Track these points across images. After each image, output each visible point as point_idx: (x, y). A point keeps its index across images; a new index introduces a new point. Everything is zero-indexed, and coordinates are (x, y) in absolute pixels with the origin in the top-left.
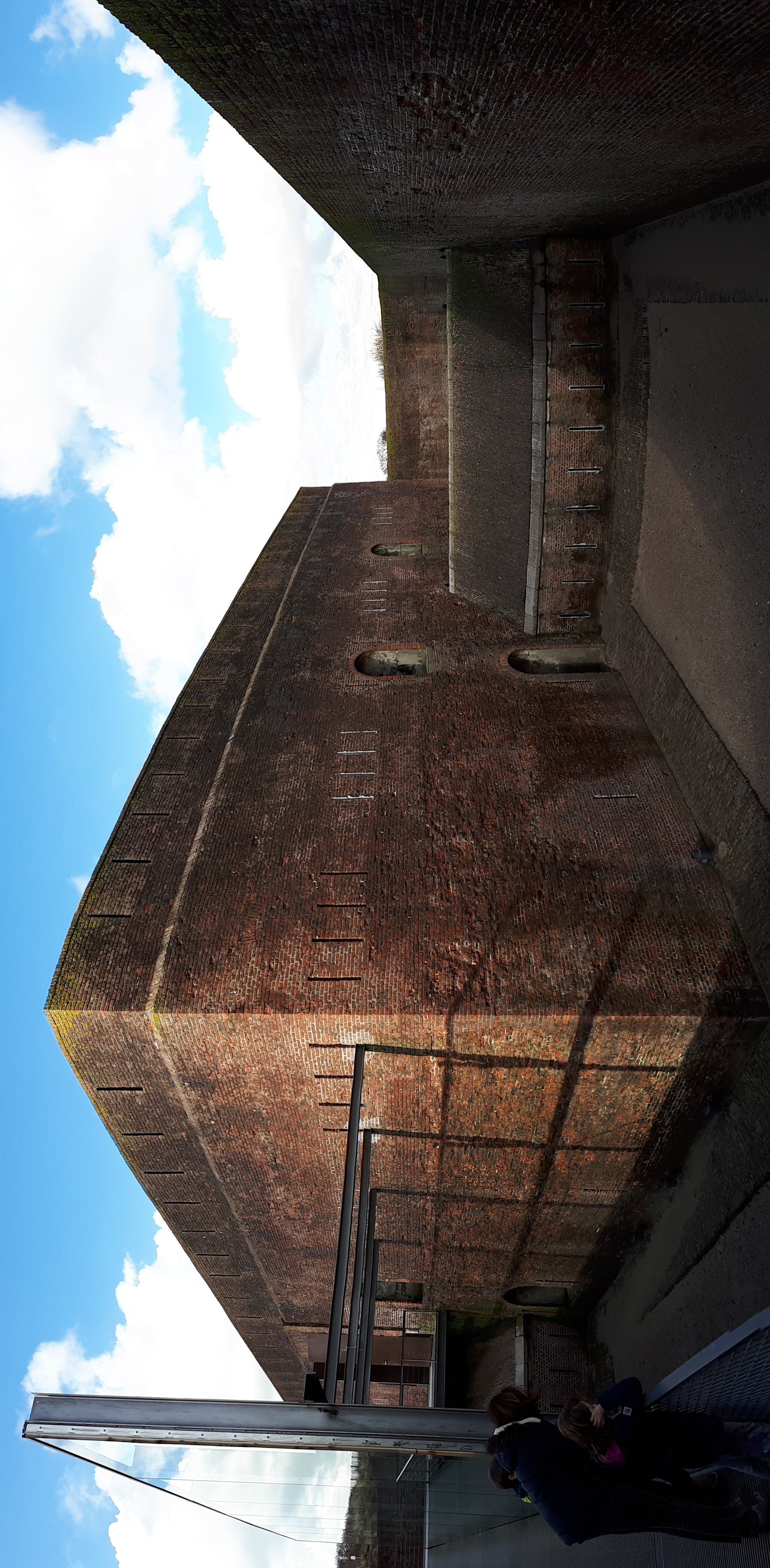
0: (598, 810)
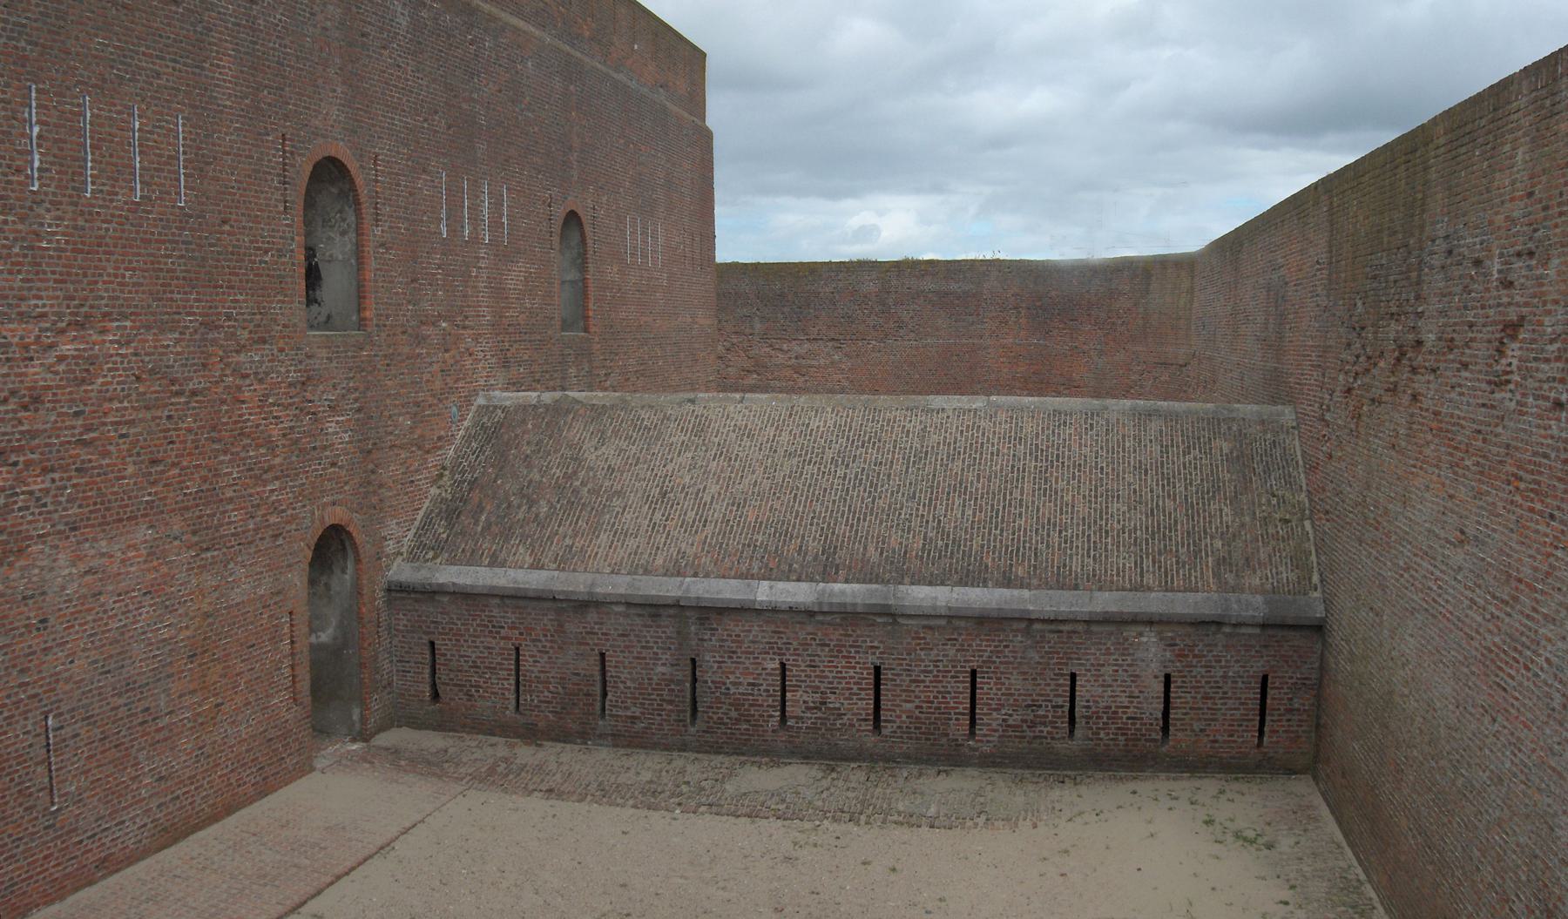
0: (22, 722)
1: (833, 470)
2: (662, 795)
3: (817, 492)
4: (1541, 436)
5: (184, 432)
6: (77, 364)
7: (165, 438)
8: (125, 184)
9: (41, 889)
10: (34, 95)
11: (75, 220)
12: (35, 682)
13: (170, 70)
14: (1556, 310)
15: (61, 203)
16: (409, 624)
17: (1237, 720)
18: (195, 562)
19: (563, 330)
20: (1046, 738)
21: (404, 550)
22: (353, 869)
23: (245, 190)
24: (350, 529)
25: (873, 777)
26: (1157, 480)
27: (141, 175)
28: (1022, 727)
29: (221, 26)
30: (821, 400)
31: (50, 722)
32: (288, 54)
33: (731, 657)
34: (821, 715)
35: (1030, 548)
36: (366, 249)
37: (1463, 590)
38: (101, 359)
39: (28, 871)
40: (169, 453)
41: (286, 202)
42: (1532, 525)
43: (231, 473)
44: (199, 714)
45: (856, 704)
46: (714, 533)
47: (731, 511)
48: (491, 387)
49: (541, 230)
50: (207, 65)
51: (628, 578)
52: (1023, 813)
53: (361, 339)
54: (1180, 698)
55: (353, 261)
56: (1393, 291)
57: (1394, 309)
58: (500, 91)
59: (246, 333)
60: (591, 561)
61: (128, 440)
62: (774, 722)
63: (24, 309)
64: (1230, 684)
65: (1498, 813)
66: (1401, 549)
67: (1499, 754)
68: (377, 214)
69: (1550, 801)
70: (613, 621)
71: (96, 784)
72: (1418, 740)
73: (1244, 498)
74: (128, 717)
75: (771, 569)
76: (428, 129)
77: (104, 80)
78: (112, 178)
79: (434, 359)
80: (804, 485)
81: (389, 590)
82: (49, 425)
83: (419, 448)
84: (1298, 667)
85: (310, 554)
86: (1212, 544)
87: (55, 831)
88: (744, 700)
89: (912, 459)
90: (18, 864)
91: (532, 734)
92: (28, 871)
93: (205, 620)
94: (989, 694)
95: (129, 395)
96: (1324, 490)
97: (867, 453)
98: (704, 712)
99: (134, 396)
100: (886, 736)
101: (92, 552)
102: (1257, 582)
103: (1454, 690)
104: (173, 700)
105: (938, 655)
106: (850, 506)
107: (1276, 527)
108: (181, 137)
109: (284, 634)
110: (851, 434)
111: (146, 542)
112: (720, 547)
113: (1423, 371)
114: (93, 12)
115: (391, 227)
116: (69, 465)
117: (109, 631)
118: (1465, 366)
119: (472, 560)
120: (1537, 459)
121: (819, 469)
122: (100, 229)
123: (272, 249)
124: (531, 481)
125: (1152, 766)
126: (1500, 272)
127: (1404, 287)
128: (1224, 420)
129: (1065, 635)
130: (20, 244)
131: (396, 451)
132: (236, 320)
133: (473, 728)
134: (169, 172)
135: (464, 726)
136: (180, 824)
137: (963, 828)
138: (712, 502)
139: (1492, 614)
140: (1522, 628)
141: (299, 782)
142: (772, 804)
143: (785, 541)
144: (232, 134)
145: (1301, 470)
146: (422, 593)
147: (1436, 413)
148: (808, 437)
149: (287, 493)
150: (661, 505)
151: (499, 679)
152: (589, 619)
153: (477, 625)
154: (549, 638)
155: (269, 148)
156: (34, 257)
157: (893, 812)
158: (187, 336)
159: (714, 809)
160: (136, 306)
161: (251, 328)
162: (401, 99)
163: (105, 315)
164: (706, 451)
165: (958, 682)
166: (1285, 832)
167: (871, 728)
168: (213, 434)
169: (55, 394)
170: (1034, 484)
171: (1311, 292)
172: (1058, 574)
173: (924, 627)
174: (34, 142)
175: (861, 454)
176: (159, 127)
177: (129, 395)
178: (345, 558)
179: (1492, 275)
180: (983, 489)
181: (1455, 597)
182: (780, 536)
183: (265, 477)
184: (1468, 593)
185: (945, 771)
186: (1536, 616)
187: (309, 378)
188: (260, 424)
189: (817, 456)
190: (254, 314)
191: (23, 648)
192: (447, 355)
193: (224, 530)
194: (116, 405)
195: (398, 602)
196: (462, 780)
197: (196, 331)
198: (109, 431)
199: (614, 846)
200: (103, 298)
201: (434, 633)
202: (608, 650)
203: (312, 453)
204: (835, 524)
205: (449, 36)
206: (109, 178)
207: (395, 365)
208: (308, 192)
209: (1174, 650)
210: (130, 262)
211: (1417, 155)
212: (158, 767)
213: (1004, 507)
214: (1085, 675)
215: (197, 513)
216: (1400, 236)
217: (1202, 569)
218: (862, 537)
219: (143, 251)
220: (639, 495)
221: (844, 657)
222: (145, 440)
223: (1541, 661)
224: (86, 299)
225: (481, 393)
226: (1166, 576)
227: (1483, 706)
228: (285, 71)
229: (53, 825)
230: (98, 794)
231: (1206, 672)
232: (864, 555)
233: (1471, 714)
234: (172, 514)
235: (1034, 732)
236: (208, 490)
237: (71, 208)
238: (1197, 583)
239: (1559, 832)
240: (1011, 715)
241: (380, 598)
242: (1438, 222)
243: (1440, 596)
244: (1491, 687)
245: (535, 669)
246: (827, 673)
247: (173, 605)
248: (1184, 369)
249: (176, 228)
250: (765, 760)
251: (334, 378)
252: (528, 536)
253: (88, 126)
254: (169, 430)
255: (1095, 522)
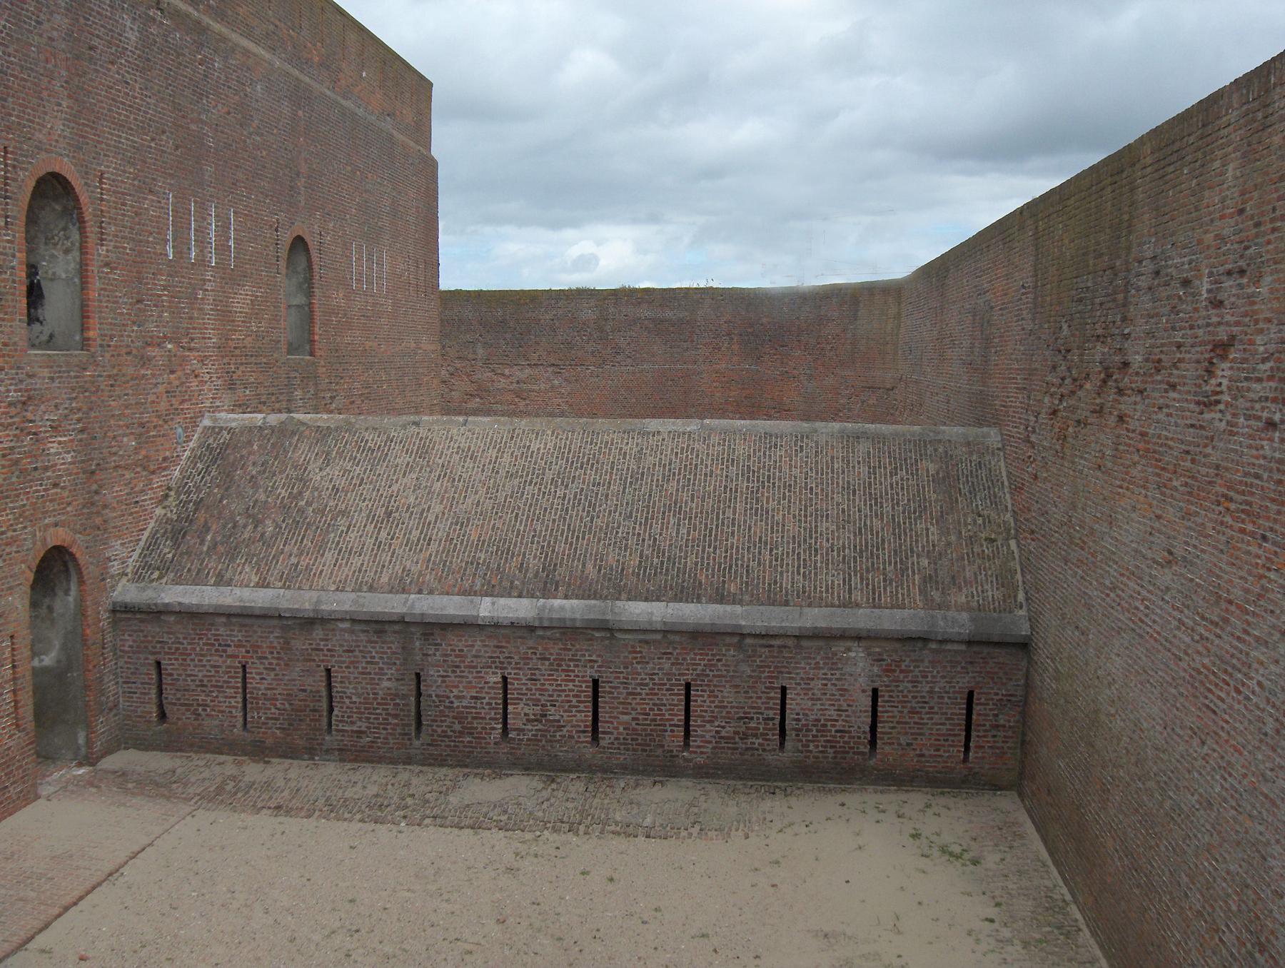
2: (389, 809)
3: (537, 512)
4: (1252, 456)
14: (1268, 329)
16: (135, 645)
17: (943, 735)
20: (757, 750)
22: (81, 898)
24: (74, 550)
25: (591, 787)
26: (865, 501)
28: (734, 738)
30: (541, 423)
33: (454, 672)
35: (742, 565)
37: (1170, 610)
41: (7, 217)
42: (1244, 546)
45: (575, 716)
46: (438, 551)
47: (455, 530)
48: (218, 409)
49: (267, 255)
51: (353, 595)
52: (735, 823)
53: (85, 360)
54: (887, 712)
55: (76, 280)
56: (1098, 313)
57: (1100, 332)
64: (936, 699)
65: (1207, 838)
66: (1108, 569)
67: (1209, 778)
68: (102, 233)
69: (1262, 828)
72: (1124, 760)
73: (950, 518)
75: (494, 586)
76: (155, 149)
79: (159, 380)
80: (525, 505)
81: (114, 611)
83: (145, 469)
84: (1003, 684)
85: (31, 576)
86: (918, 563)
89: (629, 480)
91: (260, 751)
94: (703, 706)
96: (1029, 510)
97: (585, 474)
98: (428, 725)
100: (604, 748)
102: (963, 599)
103: (1162, 711)
105: (654, 669)
106: (569, 525)
107: (982, 546)
109: (6, 659)
113: (1129, 392)
115: (115, 247)
118: (1173, 387)
120: (1249, 480)
121: (540, 489)
125: (860, 779)
126: (1209, 291)
127: (1110, 309)
128: (930, 442)
129: (776, 649)
131: (120, 472)
133: (201, 747)
135: (192, 746)
137: (677, 838)
138: (436, 522)
139: (1201, 635)
140: (1232, 650)
142: (494, 815)
143: (507, 558)
145: (1006, 490)
147: (1143, 434)
149: (7, 515)
151: (226, 697)
154: (275, 655)
157: (610, 822)
162: (129, 117)
166: (990, 848)
167: (589, 739)
170: (746, 504)
171: (1016, 316)
172: (769, 591)
173: (640, 641)
178: (68, 581)
179: (1201, 295)
180: (697, 508)
181: (1162, 618)
182: (502, 554)
184: (1175, 613)
185: (660, 781)
186: (1247, 638)
187: (30, 398)
189: (537, 477)
192: (172, 376)
195: (123, 623)
202: (334, 667)
203: (33, 473)
204: (555, 543)
205: (178, 55)
207: (119, 386)
208: (30, 207)
209: (881, 665)
211: (1124, 176)
213: (717, 526)
214: (795, 689)
216: (1106, 258)
217: (908, 586)
221: (563, 670)
223: (1253, 684)
225: (207, 414)
226: (874, 593)
227: (1191, 729)
231: (913, 687)
233: (1179, 735)
235: (746, 743)
238: (903, 600)
239: (1272, 862)
240: (723, 727)
242: (1145, 243)
243: (1147, 615)
244: (1200, 709)
246: (547, 687)
248: (891, 392)
250: (487, 772)
251: (56, 398)
252: (254, 555)
255: (805, 540)
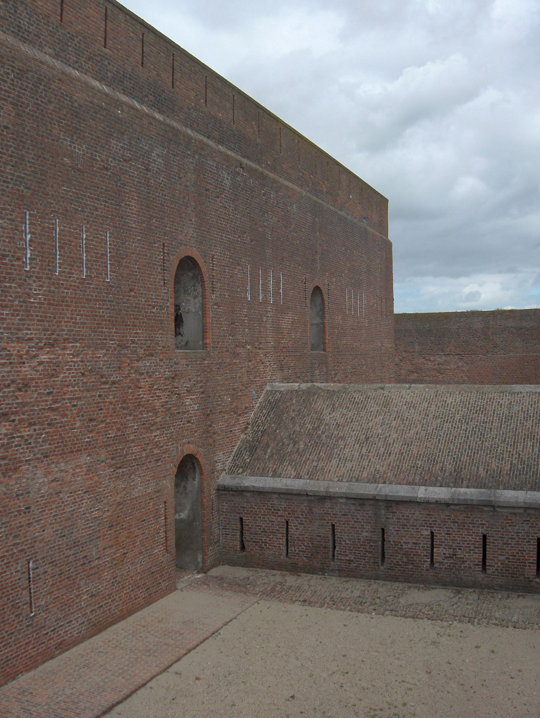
0: (15, 566)
1: (460, 426)
2: (366, 604)
3: (451, 438)
5: (107, 404)
6: (49, 366)
7: (98, 407)
8: (77, 268)
9: (24, 663)
10: (28, 217)
11: (50, 287)
12: (23, 542)
13: (103, 206)
15: (42, 278)
16: (229, 508)
18: (113, 475)
19: (312, 350)
21: (226, 468)
22: (197, 645)
23: (142, 273)
24: (198, 456)
25: (482, 597)
27: (86, 264)
29: (130, 183)
31: (31, 565)
32: (166, 199)
33: (403, 528)
34: (454, 562)
36: (207, 306)
38: (63, 364)
39: (16, 652)
40: (100, 415)
41: (164, 280)
43: (134, 426)
44: (114, 559)
45: (473, 556)
46: (394, 460)
47: (404, 448)
48: (273, 381)
49: (300, 297)
50: (123, 205)
51: (347, 484)
53: (204, 355)
58: (279, 221)
59: (142, 350)
60: (327, 474)
61: (77, 408)
62: (427, 564)
63: (20, 335)
68: (213, 288)
70: (339, 507)
71: (56, 600)
74: (75, 561)
75: (426, 480)
76: (240, 242)
77: (67, 211)
78: (70, 265)
81: (218, 490)
82: (33, 400)
83: (235, 413)
85: (176, 470)
87: (33, 628)
88: (411, 552)
89: (504, 420)
90: (11, 648)
92: (16, 652)
93: (118, 506)
95: (78, 384)
97: (478, 417)
99: (81, 384)
100: (489, 574)
101: (56, 469)
104: (100, 551)
108: (108, 243)
109: (162, 514)
110: (470, 406)
111: (86, 463)
112: (398, 468)
114: (61, 172)
115: (220, 295)
116: (44, 421)
117: (64, 513)
119: (263, 473)
121: (452, 425)
122: (63, 292)
123: (157, 306)
124: (295, 431)
130: (18, 299)
132: (137, 344)
133: (263, 566)
134: (102, 262)
135: (258, 564)
136: (103, 621)
138: (393, 443)
141: (169, 596)
142: (425, 610)
143: (433, 464)
144: (136, 243)
146: (236, 491)
148: (446, 408)
149: (164, 437)
150: (366, 445)
151: (277, 538)
152: (326, 506)
153: (266, 509)
155: (155, 251)
156: (26, 307)
158: (110, 352)
159: (394, 613)
160: (82, 335)
161: (145, 348)
163: (65, 340)
164: (390, 415)
165: (531, 545)
168: (124, 405)
169: (36, 383)
173: (511, 513)
174: (28, 243)
175: (475, 417)
176: (96, 238)
177: (78, 384)
178: (195, 472)
182: (431, 461)
183: (151, 428)
185: (522, 596)
187: (176, 375)
188: (149, 400)
189: (451, 418)
190: (147, 340)
191: (16, 524)
192: (250, 363)
193: (129, 457)
194: (71, 389)
196: (257, 594)
197: (115, 349)
198: (66, 403)
199: (340, 633)
200: (64, 330)
201: (242, 513)
204: (461, 456)
206: (68, 265)
207: (222, 369)
208: (176, 275)
210: (80, 311)
212: (91, 589)
215: (115, 448)
218: (476, 463)
219: (86, 305)
220: (353, 439)
221: (465, 529)
222: (87, 408)
224: (55, 331)
225: (268, 383)
228: (165, 209)
229: (32, 624)
230: (57, 605)
232: (477, 473)
234: (101, 449)
236: (121, 435)
237: (47, 281)
241: (213, 494)
245: (297, 533)
247: (101, 498)
249: (105, 293)
251: (190, 375)
252: (293, 461)
253: (58, 236)
254: (100, 403)
